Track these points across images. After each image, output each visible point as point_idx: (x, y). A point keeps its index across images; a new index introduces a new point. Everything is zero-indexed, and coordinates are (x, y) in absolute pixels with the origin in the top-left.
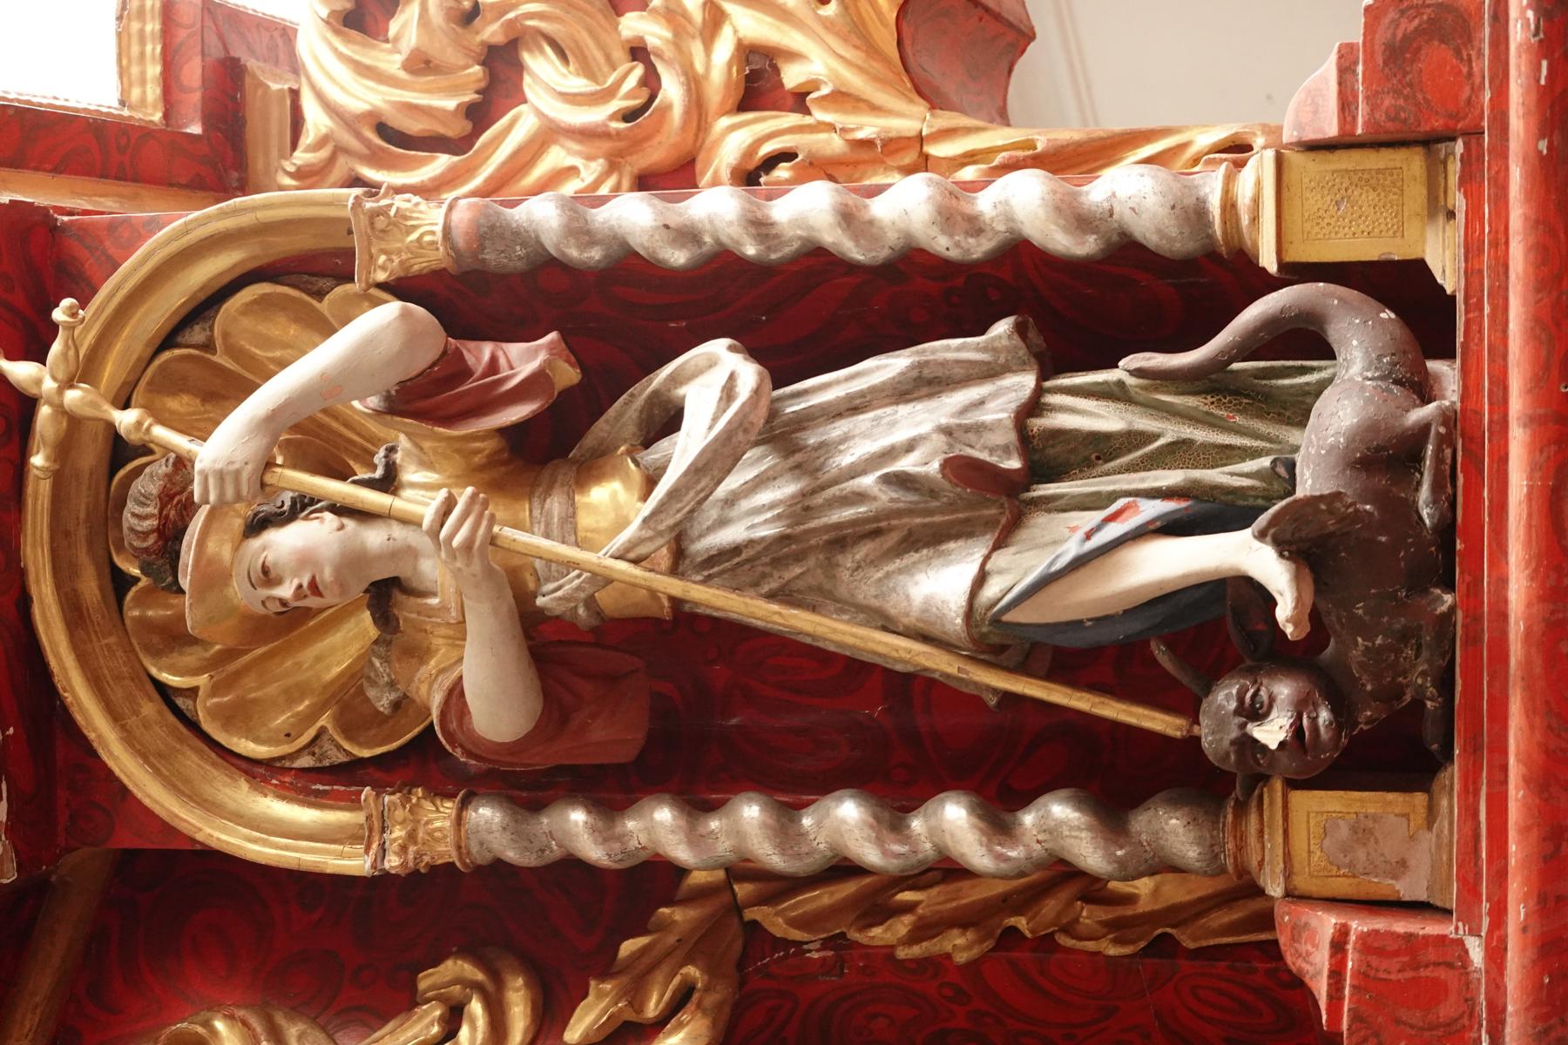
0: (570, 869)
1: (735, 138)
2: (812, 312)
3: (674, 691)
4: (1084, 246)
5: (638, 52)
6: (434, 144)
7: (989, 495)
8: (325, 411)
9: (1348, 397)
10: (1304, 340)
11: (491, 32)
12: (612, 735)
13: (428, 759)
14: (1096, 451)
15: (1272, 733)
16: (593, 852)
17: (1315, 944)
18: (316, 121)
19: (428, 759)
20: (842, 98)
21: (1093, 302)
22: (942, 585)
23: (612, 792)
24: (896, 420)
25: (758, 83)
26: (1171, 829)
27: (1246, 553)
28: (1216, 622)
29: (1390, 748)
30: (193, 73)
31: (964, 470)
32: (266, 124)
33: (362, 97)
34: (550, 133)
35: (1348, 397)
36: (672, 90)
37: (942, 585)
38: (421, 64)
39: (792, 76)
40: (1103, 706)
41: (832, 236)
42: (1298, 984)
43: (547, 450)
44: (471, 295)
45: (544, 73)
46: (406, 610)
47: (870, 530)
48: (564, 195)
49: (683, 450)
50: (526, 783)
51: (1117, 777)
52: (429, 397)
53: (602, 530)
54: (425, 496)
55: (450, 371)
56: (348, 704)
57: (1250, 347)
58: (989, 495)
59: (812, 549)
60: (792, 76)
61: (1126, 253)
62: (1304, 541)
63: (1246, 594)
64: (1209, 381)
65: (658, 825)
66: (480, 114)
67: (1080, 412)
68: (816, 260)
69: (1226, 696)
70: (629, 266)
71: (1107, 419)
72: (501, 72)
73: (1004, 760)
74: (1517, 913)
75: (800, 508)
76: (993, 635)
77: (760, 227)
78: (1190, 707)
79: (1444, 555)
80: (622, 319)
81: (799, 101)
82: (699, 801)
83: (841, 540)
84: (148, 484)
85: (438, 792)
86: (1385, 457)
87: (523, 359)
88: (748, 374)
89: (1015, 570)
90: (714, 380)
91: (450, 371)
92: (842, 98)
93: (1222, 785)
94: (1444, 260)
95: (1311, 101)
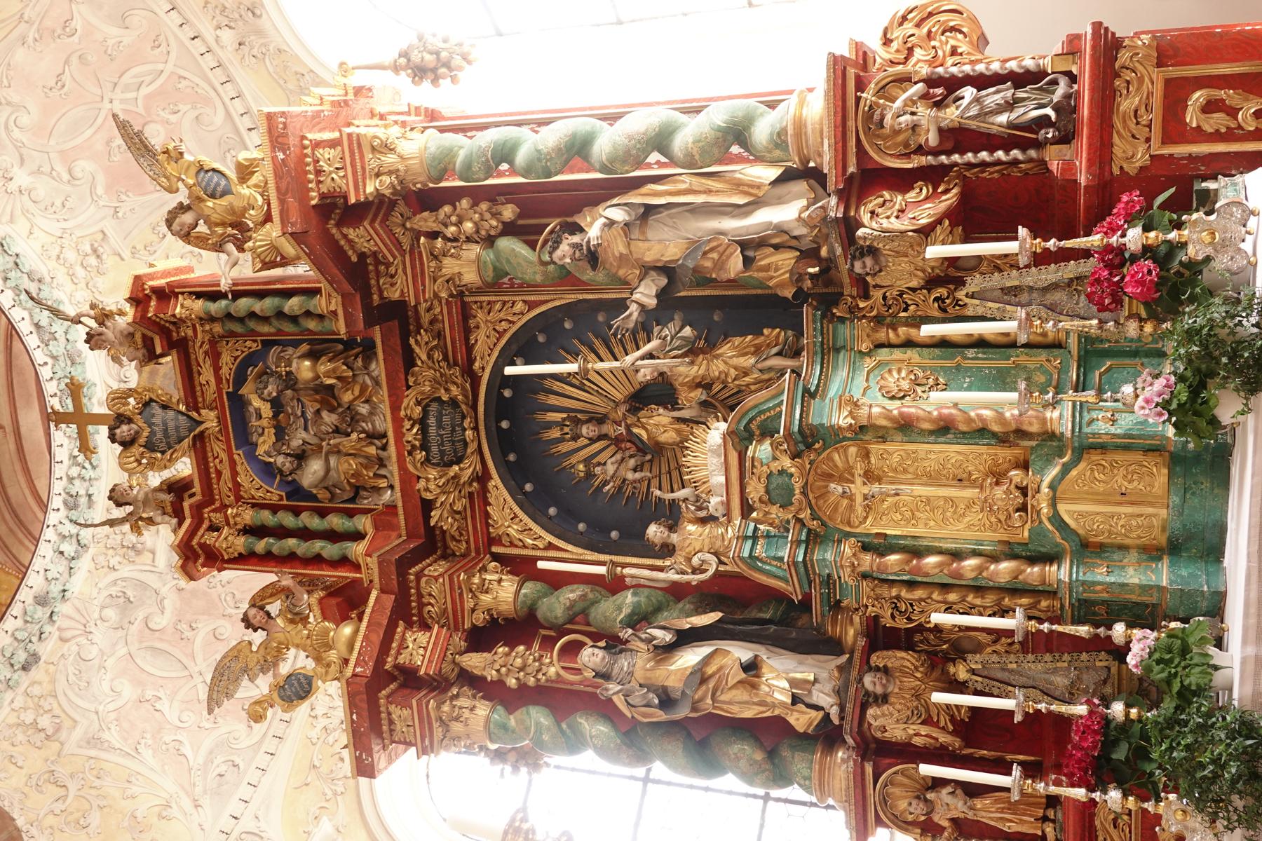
0: (942, 165)
1: (950, 61)
2: (982, 82)
3: (957, 138)
4: (1021, 71)
5: (934, 47)
6: (899, 64)
7: (1010, 105)
8: (234, 285)
9: (1061, 90)
10: (1055, 82)
11: (909, 45)
12: (949, 145)
13: (920, 150)
14: (1024, 99)
15: (1050, 136)
16: (946, 162)
17: (1054, 166)
18: (879, 60)
19: (920, 150)
20: (969, 53)
21: (1022, 79)
22: (1003, 118)
23: (949, 153)
24: (994, 97)
25: (954, 52)
26: (1032, 153)
27: (1049, 111)
28: (1043, 122)
29: (1065, 138)
30: (861, 53)
31: (1007, 102)
32: (870, 61)
33: (887, 56)
34: (919, 61)
35: (1061, 90)
36: (940, 53)
37: (1003, 118)
38: (898, 51)
39: (959, 50)
40: (1024, 136)
41: (984, 71)
42: (1051, 172)
43: (939, 105)
44: (931, 82)
45: (918, 51)
46: (918, 129)
47: (991, 112)
48: (952, 68)
49: (965, 102)
50: (935, 153)
51: (1024, 145)
52: (925, 96)
53: (952, 114)
54: (924, 113)
55: (928, 93)
56: (906, 145)
57: (1047, 84)
58: (1010, 105)
59: (983, 115)
60: (959, 50)
61: (1028, 72)
62: (1056, 109)
63: (1047, 117)
64: (1040, 89)
65: (956, 157)
66: (907, 59)
67: (1021, 94)
68: (981, 75)
69: (1043, 132)
70: (953, 76)
71: (1025, 95)
72: (910, 51)
73: (1007, 143)
74: (1084, 155)
75: (981, 109)
76: (1011, 125)
77: (974, 70)
78: (1037, 133)
79: (1075, 110)
80: (953, 85)
81: (961, 54)
82: (962, 153)
83: (986, 114)
84: (878, 112)
85: (922, 155)
86: (1068, 96)
87: (939, 91)
88: (975, 91)
89: (1013, 116)
90: (968, 92)
91: (928, 93)
92: (969, 53)
93: (1038, 145)
94: (1075, 70)
95: (1058, 49)
